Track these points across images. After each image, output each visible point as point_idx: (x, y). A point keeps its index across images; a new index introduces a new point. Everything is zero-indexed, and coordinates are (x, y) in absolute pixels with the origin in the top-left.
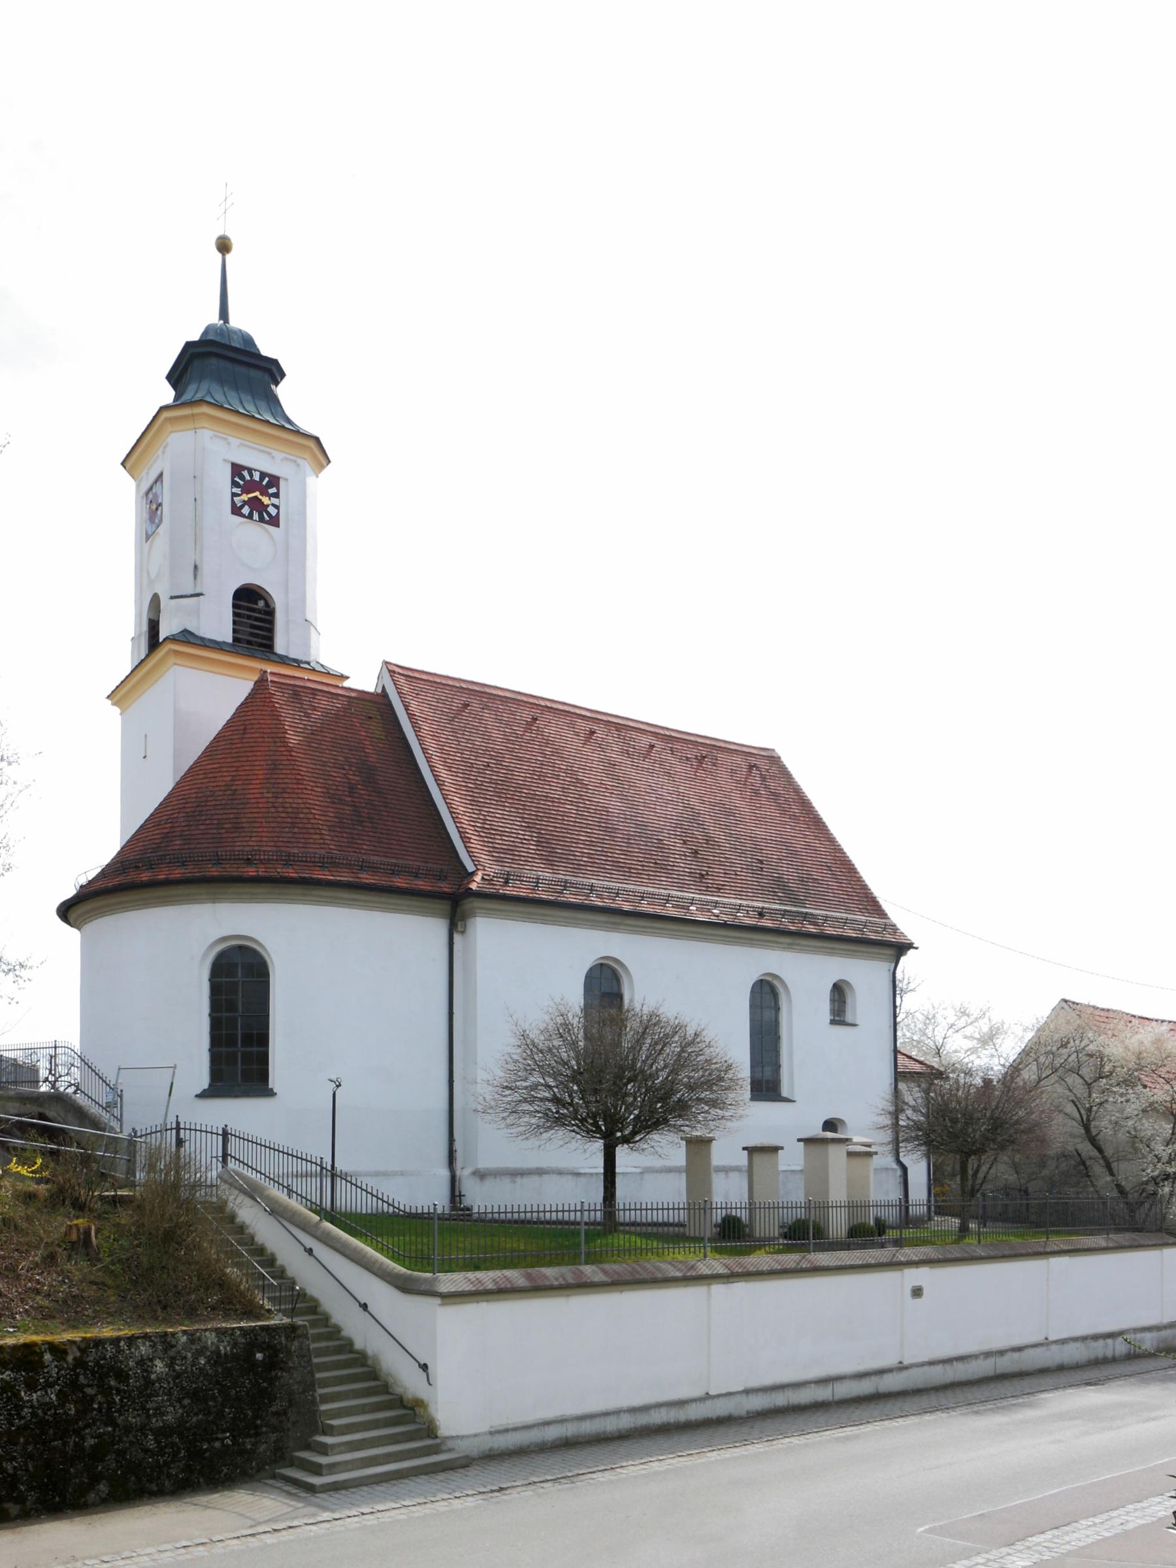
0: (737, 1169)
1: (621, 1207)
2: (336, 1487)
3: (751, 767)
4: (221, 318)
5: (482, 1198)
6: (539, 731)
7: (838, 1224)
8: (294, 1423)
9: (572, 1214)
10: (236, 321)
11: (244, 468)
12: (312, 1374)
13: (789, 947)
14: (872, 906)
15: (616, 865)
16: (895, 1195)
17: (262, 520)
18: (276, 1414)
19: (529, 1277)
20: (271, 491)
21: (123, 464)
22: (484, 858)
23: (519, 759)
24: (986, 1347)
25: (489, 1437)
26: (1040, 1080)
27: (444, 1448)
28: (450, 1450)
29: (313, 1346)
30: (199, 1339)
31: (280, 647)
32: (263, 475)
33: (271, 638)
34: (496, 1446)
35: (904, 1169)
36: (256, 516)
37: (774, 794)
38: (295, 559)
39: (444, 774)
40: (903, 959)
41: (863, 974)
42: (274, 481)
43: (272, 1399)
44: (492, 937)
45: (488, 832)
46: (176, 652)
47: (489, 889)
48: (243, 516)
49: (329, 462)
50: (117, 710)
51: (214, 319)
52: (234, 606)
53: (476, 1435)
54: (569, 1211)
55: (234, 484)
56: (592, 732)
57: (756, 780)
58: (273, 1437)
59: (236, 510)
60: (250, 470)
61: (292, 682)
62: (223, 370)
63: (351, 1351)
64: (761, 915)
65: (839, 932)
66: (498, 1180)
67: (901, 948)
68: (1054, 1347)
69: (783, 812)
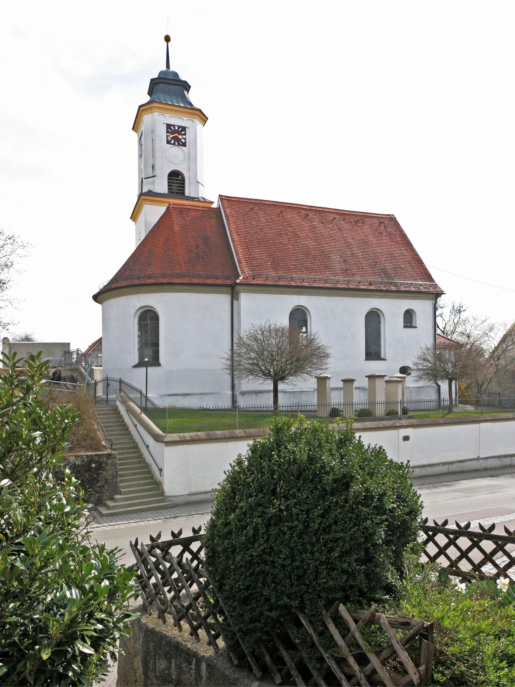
0: (268, 392)
1: (281, 405)
2: (112, 515)
3: (381, 223)
4: (167, 68)
5: (243, 402)
6: (283, 217)
7: (380, 410)
8: (107, 490)
9: (303, 407)
10: (173, 68)
11: (171, 125)
12: (117, 472)
13: (383, 297)
14: (429, 277)
15: (307, 268)
16: (434, 396)
17: (179, 145)
18: (100, 487)
19: (245, 432)
20: (182, 133)
21: (133, 129)
22: (246, 270)
23: (271, 229)
24: (444, 460)
25: (188, 496)
26: (507, 348)
27: (166, 500)
28: (169, 501)
29: (118, 462)
30: (67, 459)
31: (187, 194)
32: (179, 127)
33: (184, 190)
34: (191, 499)
35: (439, 387)
36: (176, 144)
37: (389, 233)
38: (192, 159)
39: (236, 237)
40: (438, 299)
41: (421, 307)
42: (184, 129)
43: (98, 481)
44: (247, 300)
45: (250, 259)
46: (145, 200)
47: (245, 282)
48: (171, 144)
49: (207, 119)
50: (134, 223)
51: (164, 68)
52: (169, 179)
53: (181, 496)
54: (285, 407)
55: (168, 132)
56: (307, 215)
57: (382, 228)
58: (97, 495)
59: (168, 142)
60: (174, 126)
61: (180, 207)
62: (168, 88)
63: (145, 463)
64: (370, 284)
65: (407, 289)
66: (250, 395)
67: (439, 294)
68: (481, 461)
69: (392, 240)
